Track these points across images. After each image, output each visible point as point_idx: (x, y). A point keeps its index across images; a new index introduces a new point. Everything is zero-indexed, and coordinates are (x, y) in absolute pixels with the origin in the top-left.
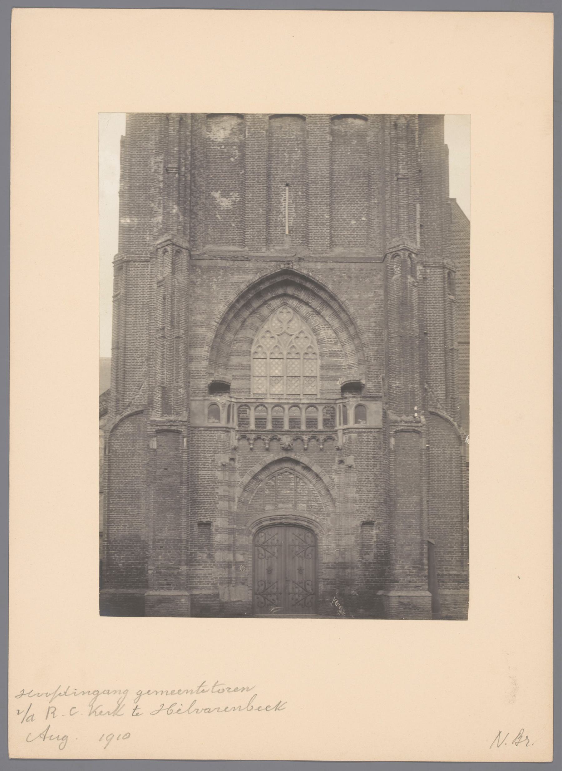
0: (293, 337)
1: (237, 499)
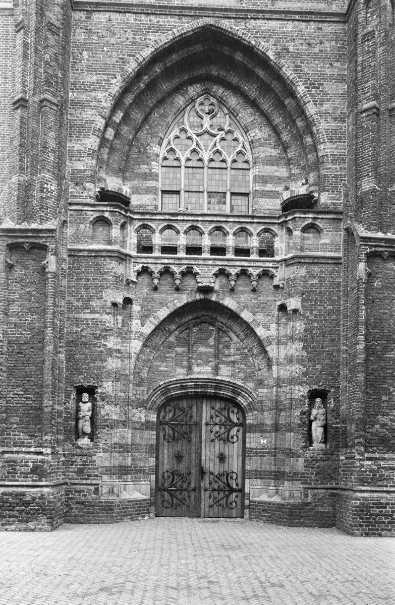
0: (218, 137)
1: (134, 356)
